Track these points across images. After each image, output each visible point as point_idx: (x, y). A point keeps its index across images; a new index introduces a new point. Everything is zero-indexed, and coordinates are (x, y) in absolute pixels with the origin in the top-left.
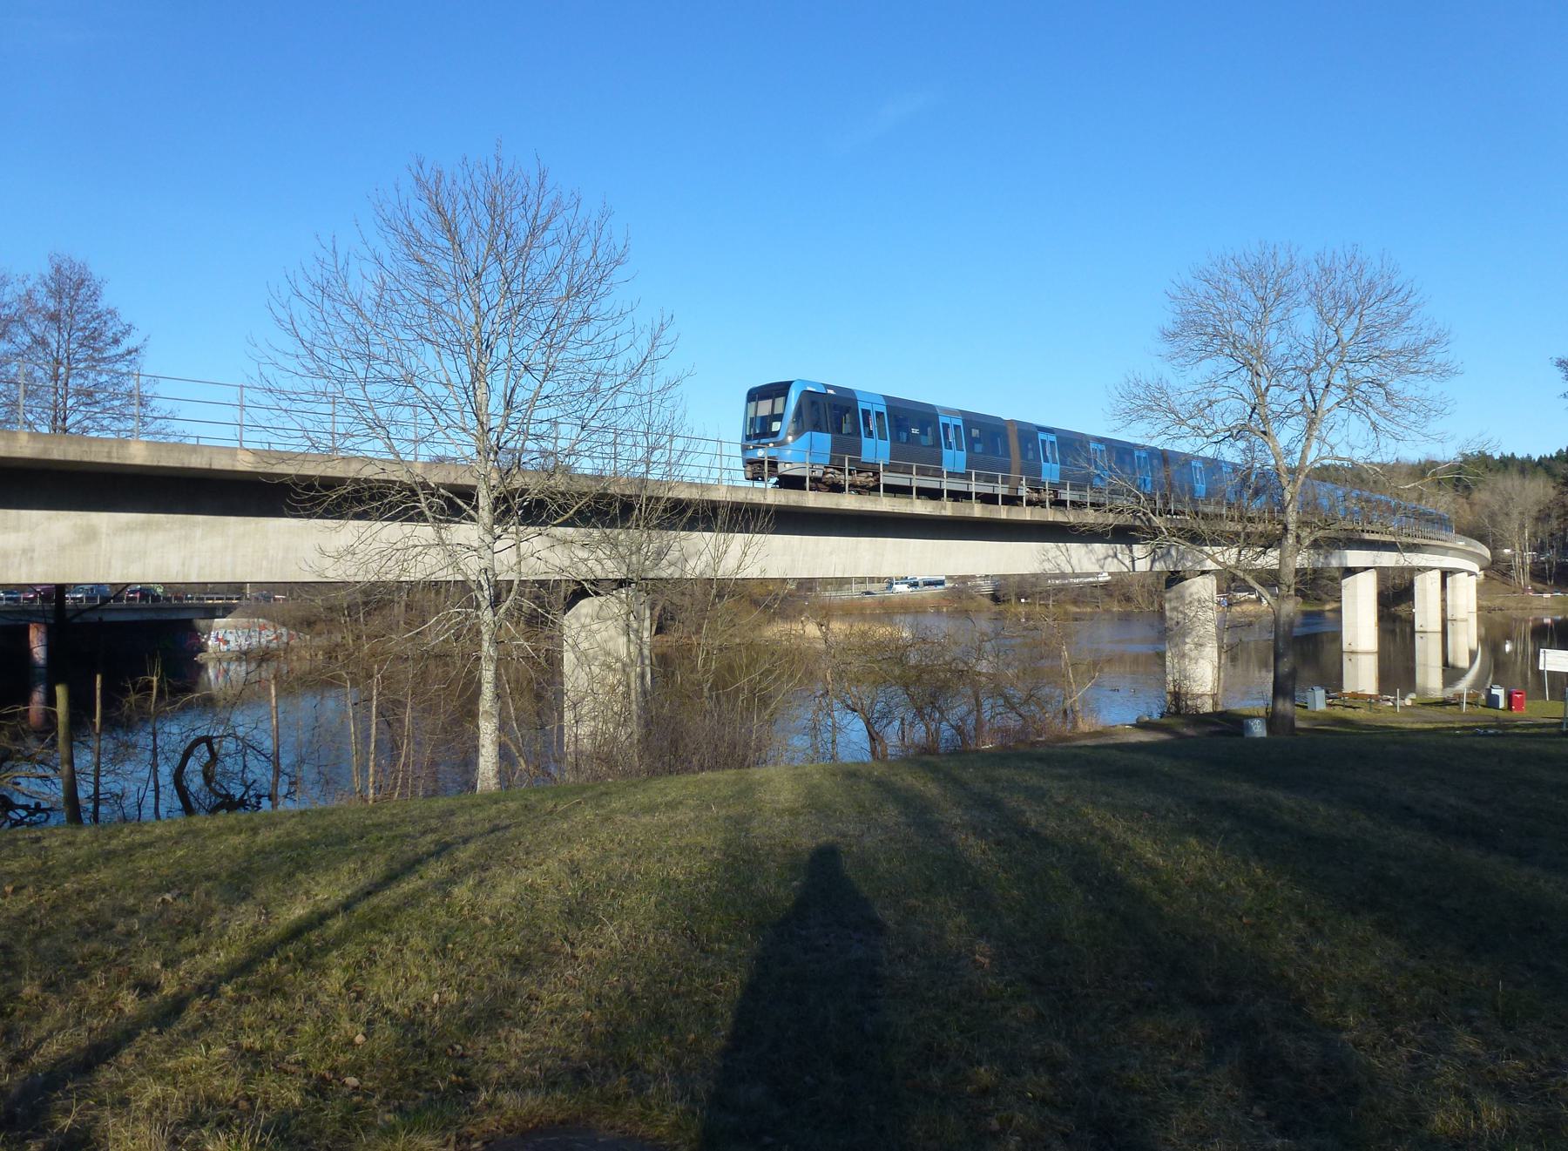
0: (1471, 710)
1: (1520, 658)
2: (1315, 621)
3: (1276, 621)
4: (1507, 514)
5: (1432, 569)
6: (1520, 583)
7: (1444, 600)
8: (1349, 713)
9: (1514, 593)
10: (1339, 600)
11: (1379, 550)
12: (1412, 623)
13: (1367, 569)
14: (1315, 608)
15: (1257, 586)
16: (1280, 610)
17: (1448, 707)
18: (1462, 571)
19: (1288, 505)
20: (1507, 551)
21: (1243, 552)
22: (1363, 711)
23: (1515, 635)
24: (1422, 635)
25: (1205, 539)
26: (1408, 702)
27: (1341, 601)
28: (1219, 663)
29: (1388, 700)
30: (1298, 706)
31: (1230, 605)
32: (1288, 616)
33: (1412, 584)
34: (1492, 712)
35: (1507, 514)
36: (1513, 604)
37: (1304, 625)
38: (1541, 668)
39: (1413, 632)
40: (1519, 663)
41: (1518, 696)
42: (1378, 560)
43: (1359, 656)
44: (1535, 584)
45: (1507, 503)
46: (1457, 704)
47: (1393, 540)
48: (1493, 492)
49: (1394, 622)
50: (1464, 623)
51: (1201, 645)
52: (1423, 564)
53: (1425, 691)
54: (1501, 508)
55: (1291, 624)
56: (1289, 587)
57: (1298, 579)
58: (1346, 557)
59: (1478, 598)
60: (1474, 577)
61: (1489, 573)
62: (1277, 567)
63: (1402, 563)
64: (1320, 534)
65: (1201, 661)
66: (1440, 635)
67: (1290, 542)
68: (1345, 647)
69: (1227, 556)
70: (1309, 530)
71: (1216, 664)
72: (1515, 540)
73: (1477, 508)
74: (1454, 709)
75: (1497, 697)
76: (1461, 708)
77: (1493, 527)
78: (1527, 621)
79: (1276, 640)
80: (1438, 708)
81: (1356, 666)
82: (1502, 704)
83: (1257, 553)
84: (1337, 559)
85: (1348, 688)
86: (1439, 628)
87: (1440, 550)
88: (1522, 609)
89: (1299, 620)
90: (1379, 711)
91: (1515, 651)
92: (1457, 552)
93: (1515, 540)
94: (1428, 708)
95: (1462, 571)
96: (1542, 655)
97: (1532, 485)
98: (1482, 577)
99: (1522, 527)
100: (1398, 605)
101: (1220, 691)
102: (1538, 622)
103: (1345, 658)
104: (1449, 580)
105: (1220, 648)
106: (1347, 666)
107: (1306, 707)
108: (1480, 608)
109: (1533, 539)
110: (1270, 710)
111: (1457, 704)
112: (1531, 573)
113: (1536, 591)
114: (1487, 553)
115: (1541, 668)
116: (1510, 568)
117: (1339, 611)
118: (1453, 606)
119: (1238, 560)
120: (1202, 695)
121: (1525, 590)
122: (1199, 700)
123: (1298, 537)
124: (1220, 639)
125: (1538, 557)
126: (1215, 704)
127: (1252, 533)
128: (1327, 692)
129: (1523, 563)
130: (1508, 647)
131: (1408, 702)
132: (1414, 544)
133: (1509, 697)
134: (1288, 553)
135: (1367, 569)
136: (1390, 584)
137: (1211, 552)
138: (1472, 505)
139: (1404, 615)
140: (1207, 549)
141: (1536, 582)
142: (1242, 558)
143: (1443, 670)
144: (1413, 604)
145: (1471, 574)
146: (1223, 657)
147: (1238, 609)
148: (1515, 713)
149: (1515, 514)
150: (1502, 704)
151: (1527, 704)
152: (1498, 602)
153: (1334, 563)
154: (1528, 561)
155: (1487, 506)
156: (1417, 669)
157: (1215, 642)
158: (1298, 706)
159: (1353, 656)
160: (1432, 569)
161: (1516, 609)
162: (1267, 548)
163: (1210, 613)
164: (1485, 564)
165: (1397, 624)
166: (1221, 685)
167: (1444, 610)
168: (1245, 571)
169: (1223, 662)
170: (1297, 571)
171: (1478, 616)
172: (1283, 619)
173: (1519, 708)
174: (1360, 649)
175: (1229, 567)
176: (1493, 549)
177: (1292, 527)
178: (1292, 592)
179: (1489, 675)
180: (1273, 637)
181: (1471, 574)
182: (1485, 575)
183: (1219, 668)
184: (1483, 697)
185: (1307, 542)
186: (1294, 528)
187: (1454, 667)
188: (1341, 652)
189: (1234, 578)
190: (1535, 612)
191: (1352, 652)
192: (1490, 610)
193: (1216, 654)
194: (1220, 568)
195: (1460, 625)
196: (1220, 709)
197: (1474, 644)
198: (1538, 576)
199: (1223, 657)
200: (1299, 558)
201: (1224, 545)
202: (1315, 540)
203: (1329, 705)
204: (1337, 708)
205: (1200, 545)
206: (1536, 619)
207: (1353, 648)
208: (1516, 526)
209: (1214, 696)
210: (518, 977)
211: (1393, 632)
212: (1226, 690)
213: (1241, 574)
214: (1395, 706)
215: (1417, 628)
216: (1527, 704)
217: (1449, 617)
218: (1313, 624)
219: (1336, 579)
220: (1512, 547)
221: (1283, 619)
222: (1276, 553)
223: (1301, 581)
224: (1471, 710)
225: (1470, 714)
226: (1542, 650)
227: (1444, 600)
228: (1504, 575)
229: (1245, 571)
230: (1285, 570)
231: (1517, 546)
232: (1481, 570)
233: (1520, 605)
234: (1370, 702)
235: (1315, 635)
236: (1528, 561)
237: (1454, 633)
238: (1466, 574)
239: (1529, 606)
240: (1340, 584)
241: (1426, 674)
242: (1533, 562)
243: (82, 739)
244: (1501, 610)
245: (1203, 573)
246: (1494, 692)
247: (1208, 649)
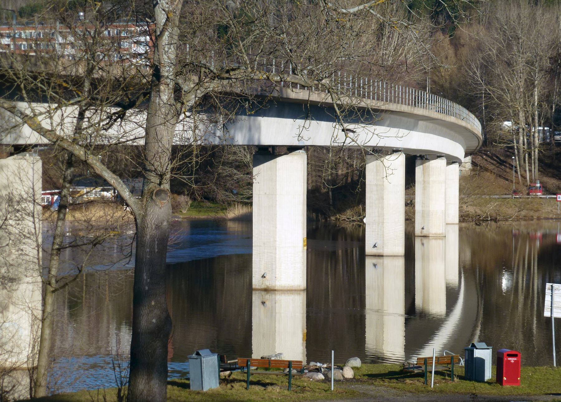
0: (442, 385)
1: (521, 298)
2: (211, 237)
3: (138, 237)
4: (509, 64)
5: (395, 151)
6: (524, 177)
7: (410, 204)
8: (256, 393)
9: (515, 192)
10: (248, 202)
11: (306, 117)
12: (362, 240)
13: (291, 149)
14: (212, 215)
15: (108, 175)
16: (144, 217)
17: (408, 381)
18: (439, 156)
19: (162, 32)
20: (153, 303)
21: (87, 114)
22: (277, 389)
23: (516, 259)
24: (374, 260)
25: (18, 88)
26: (348, 373)
27: (251, 204)
28: (44, 311)
29: (318, 370)
30: (173, 383)
31: (62, 207)
32: (158, 227)
33: (362, 174)
34: (468, 386)
35: (509, 64)
36: (512, 211)
37: (193, 244)
38: (547, 314)
39: (363, 255)
40: (520, 306)
41: (512, 360)
42: (305, 134)
43: (386, 261)
44: (546, 179)
45: (509, 46)
46: (422, 375)
47: (329, 100)
48: (489, 26)
49: (335, 238)
50: (440, 242)
51: (12, 280)
52: (374, 142)
53: (378, 359)
54: (500, 52)
55: (163, 240)
56: (161, 176)
57: (176, 163)
58: (259, 128)
59: (462, 201)
60: (456, 166)
61: (479, 160)
62: (142, 142)
63: (341, 139)
64: (213, 86)
65: (11, 308)
66: (400, 263)
67: (165, 97)
68: (256, 281)
69: (57, 118)
70: (195, 78)
71: (39, 314)
72: (519, 106)
73: (464, 51)
74: (418, 383)
75: (482, 362)
76: (426, 383)
77: (489, 83)
78: (532, 239)
79: (138, 271)
80: (394, 383)
81: (272, 315)
82: (488, 374)
83: (110, 117)
84: (245, 131)
85: (258, 352)
86: (400, 249)
87: (405, 119)
88: (526, 218)
89: (184, 232)
90: (303, 389)
91: (515, 288)
92: (430, 125)
93: (519, 106)
94: (378, 382)
95: (439, 156)
96: (548, 292)
97: (547, 16)
98: (469, 166)
99: (530, 84)
100: (341, 211)
101: (44, 362)
102: (549, 241)
103: (256, 299)
104: (419, 170)
105: (46, 283)
106: (258, 312)
107: (186, 386)
108: (463, 218)
109: (545, 105)
110: (125, 391)
111: (422, 375)
112: (540, 160)
113: (546, 190)
114: (476, 126)
115: (547, 314)
116: (510, 151)
117: (247, 220)
118: (425, 214)
119: (78, 129)
120: (13, 369)
121: (531, 189)
122: (7, 379)
123: (177, 91)
124: (45, 270)
125: (552, 134)
126: (34, 385)
127: (101, 80)
128: (221, 359)
129: (529, 143)
130: (505, 282)
131: (348, 373)
132: (360, 109)
133: (498, 361)
134: (159, 120)
135: (291, 149)
136: (327, 174)
137: (28, 112)
138: (456, 44)
139: (349, 227)
140: (23, 106)
141: (547, 175)
142: (85, 124)
143: (407, 320)
144: (364, 210)
145: (451, 160)
146: (50, 300)
147: (78, 215)
148: (507, 388)
149: (520, 65)
150: (488, 374)
151: (526, 372)
152: (490, 208)
153: (240, 138)
154: (537, 142)
155: (480, 48)
156: (368, 317)
157: (36, 274)
158: (173, 383)
159: (267, 297)
160: (395, 151)
161: (518, 219)
162: (126, 107)
163: (28, 222)
164: (474, 144)
165: (340, 243)
166: (46, 351)
167: (410, 220)
168: (87, 147)
169: (49, 309)
170: (175, 149)
171: (460, 230)
172: (150, 232)
173: (513, 380)
174: (386, 252)
175: (59, 138)
176: (486, 121)
177: (167, 71)
178: (166, 186)
179: (475, 327)
180: (132, 265)
181: (451, 160)
182: (474, 163)
183: (43, 320)
184: (462, 362)
185: (191, 100)
186: (171, 75)
187: (424, 315)
188: (250, 289)
189: (72, 161)
190: (545, 224)
191: (267, 290)
192: (479, 220)
193: (38, 296)
194: (45, 141)
195: (434, 245)
196: (42, 393)
197: (453, 276)
198: (549, 166)
199: (50, 300)
200: (179, 127)
201: (53, 100)
202: (206, 97)
203: (224, 381)
204: (237, 385)
205: (11, 98)
206: (544, 236)
207: (267, 283)
208: (522, 84)
209: (32, 371)
210: (16, 377)
211: (333, 255)
212: (53, 359)
213: (80, 152)
214: (327, 379)
215: (369, 249)
216: (526, 372)
217: (418, 231)
218: (207, 243)
219: (246, 166)
220: (515, 117)
221: (150, 232)
222: (142, 118)
223: (179, 169)
224: (442, 385)
225: (441, 391)
226: (548, 285)
227: (410, 204)
228: (502, 163)
229: (87, 147)
230: (155, 148)
231: (522, 115)
232: (466, 155)
233: (523, 213)
234: (289, 375)
235: (211, 261)
236: (537, 142)
237: (424, 258)
238: (442, 162)
239: (536, 215)
240: (250, 173)
241: (381, 326)
242: (544, 143)
243: (384, 379)
244: (495, 220)
245: (19, 149)
246: (478, 353)
247: (23, 287)
